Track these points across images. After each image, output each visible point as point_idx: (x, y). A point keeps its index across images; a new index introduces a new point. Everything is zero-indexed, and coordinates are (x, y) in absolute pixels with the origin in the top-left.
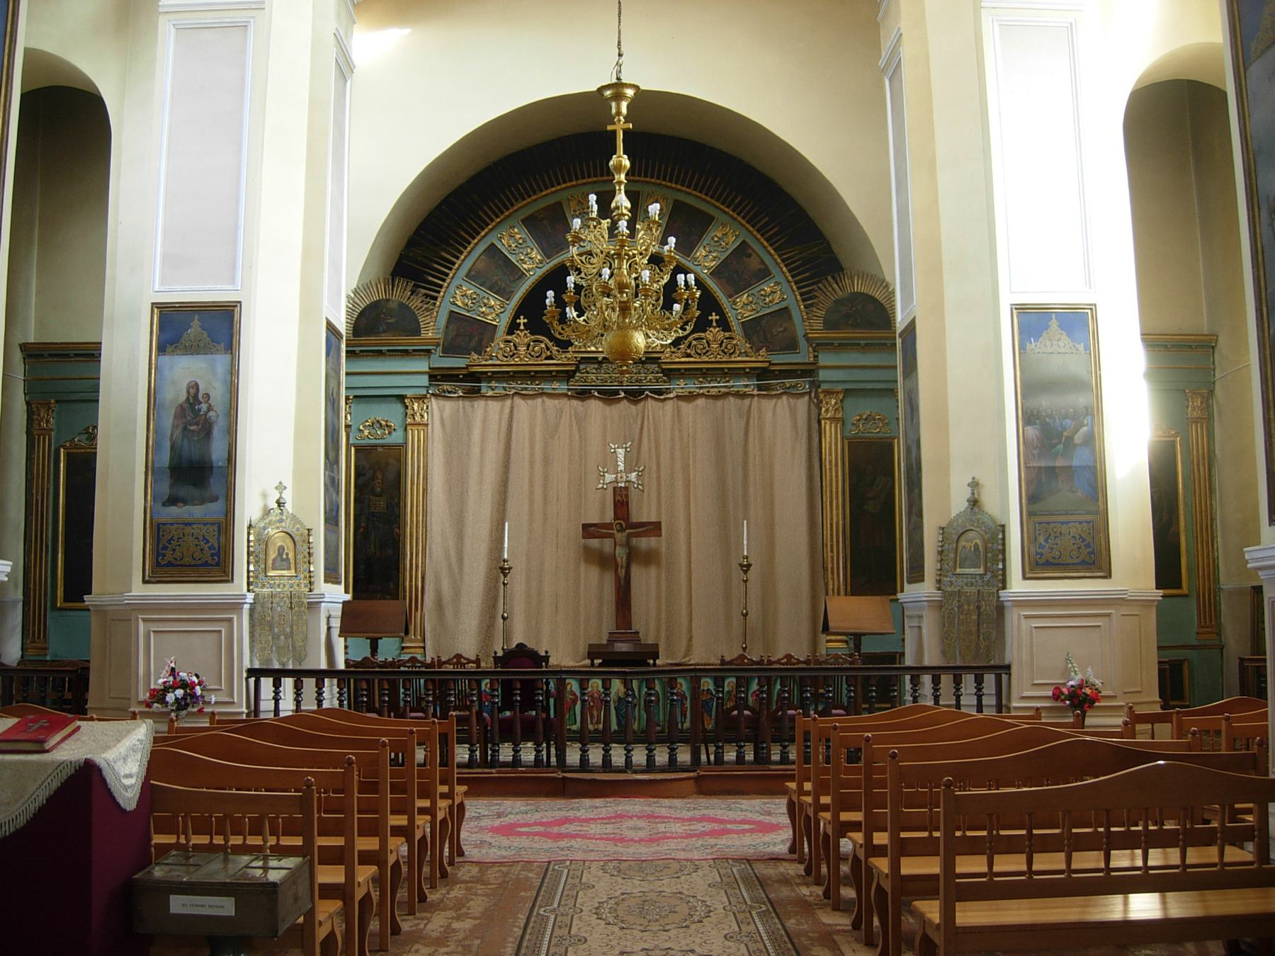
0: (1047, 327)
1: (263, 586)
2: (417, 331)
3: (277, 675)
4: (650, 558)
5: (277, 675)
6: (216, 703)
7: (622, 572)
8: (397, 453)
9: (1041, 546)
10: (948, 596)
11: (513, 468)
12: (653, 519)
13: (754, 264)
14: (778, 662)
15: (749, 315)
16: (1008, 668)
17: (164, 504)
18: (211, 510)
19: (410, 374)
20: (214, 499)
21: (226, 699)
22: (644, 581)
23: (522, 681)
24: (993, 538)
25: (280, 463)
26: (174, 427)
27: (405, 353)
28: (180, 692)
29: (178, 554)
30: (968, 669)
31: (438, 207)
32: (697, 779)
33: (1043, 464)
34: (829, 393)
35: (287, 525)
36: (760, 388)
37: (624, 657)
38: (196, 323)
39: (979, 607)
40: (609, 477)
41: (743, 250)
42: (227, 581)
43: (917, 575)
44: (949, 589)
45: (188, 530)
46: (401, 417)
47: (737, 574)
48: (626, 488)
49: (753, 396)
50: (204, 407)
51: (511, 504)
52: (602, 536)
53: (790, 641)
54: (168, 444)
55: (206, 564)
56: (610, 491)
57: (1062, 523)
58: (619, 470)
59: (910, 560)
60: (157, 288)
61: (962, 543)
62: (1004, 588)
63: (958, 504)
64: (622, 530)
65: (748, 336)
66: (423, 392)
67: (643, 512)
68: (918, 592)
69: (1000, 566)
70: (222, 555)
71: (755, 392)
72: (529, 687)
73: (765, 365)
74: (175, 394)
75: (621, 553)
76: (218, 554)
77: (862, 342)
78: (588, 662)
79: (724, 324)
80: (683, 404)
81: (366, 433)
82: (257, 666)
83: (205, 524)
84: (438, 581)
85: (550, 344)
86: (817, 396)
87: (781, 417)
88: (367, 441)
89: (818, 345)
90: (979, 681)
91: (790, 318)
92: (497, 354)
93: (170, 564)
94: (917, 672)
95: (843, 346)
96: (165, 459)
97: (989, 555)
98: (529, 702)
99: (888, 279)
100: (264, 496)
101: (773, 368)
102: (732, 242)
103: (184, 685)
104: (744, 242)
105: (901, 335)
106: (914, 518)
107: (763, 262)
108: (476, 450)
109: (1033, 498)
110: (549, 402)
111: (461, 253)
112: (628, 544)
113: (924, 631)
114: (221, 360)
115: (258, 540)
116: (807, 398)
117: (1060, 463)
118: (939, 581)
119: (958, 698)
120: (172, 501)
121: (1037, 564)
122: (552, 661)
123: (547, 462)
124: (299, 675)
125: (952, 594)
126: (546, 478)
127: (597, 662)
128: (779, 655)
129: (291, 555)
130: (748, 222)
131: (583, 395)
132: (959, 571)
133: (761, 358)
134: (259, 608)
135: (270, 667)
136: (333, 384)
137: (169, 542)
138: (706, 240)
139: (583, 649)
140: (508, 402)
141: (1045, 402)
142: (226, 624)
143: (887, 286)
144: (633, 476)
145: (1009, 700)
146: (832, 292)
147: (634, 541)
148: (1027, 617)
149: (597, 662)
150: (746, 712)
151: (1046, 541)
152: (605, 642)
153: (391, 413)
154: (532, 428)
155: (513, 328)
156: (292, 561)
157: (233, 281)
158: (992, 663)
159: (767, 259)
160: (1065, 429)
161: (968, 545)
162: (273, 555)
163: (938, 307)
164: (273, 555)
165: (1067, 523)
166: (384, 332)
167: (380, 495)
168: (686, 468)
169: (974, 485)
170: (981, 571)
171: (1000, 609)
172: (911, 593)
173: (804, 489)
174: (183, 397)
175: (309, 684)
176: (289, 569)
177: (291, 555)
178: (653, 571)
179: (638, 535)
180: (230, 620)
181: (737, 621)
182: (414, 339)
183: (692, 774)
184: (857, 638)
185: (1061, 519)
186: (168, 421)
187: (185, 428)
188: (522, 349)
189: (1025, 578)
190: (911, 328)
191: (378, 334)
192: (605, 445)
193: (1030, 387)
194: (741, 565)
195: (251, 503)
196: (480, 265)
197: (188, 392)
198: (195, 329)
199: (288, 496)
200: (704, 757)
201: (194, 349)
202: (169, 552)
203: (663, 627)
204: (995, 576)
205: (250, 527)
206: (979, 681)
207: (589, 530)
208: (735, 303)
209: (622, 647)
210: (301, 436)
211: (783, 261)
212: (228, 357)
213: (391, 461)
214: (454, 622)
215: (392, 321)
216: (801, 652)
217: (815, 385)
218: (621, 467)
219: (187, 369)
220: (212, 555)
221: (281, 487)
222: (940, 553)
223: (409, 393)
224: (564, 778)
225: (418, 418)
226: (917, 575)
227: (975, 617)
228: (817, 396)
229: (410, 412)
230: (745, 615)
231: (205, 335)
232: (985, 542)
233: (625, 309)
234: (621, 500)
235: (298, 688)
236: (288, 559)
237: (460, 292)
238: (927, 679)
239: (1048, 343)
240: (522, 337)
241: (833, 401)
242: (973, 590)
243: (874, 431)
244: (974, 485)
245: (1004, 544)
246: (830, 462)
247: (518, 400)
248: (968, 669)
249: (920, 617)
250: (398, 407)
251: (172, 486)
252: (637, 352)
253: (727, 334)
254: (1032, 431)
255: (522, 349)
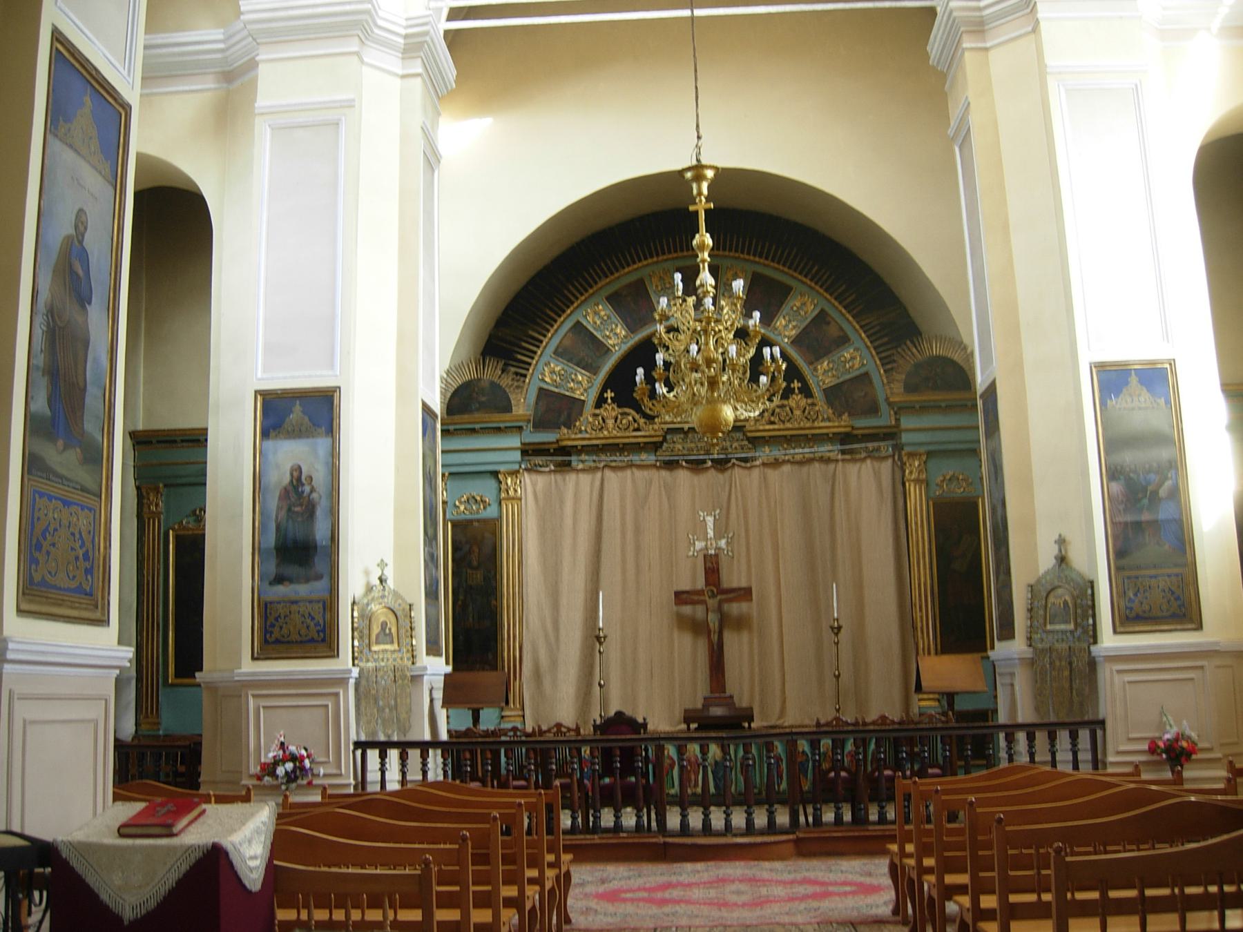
0: (1127, 383)
1: (368, 661)
2: (508, 409)
3: (383, 747)
4: (741, 623)
5: (383, 747)
6: (325, 775)
7: (715, 638)
8: (492, 528)
9: (1130, 600)
10: (1039, 653)
11: (605, 536)
12: (744, 584)
13: (833, 331)
14: (874, 723)
15: (829, 381)
16: (1102, 723)
17: (270, 584)
18: (317, 588)
19: (503, 449)
20: (319, 577)
21: (335, 771)
22: (736, 647)
23: (620, 748)
24: (1083, 594)
25: (382, 542)
26: (279, 509)
27: (498, 430)
28: (289, 766)
29: (285, 631)
30: (1063, 725)
31: (525, 288)
32: (797, 842)
33: (1129, 518)
34: (911, 455)
35: (389, 600)
36: (843, 452)
37: (720, 721)
38: (298, 408)
39: (1070, 664)
40: (699, 545)
41: (821, 318)
42: (332, 657)
43: (1007, 632)
44: (1040, 646)
45: (294, 607)
46: (495, 492)
47: (828, 636)
48: (716, 555)
49: (837, 461)
50: (307, 489)
51: (604, 572)
52: (693, 603)
53: (882, 702)
54: (273, 527)
55: (312, 640)
56: (701, 558)
57: (1151, 577)
58: (708, 536)
59: (1000, 618)
60: (259, 375)
61: (1051, 599)
62: (1095, 642)
63: (1046, 561)
64: (713, 596)
65: (830, 403)
66: (516, 467)
67: (733, 578)
68: (1010, 650)
69: (1091, 621)
70: (328, 631)
71: (840, 457)
72: (629, 755)
73: (848, 430)
74: (279, 477)
75: (713, 619)
76: (324, 631)
77: (943, 404)
78: (684, 726)
79: (806, 391)
80: (770, 472)
81: (462, 508)
82: (363, 738)
83: (311, 602)
84: (535, 651)
85: (637, 417)
86: (900, 458)
87: (865, 481)
88: (463, 517)
89: (900, 408)
90: (1074, 737)
91: (871, 382)
92: (585, 429)
93: (277, 641)
94: (1011, 730)
95: (924, 409)
96: (271, 540)
97: (1079, 611)
98: (628, 769)
99: (966, 340)
100: (367, 573)
101: (855, 432)
102: (811, 311)
103: (293, 758)
104: (822, 311)
105: (981, 396)
106: (1002, 577)
107: (841, 329)
108: (568, 521)
109: (1121, 552)
110: (639, 474)
111: (548, 331)
112: (720, 609)
113: (1017, 688)
114: (323, 443)
115: (362, 616)
116: (890, 461)
117: (1145, 517)
118: (1029, 638)
119: (1053, 754)
120: (279, 580)
121: (1127, 618)
122: (650, 727)
123: (638, 531)
124: (404, 746)
125: (1042, 650)
126: (638, 548)
127: (694, 726)
128: (872, 716)
129: (394, 630)
130: (826, 290)
131: (670, 465)
132: (1049, 627)
133: (842, 424)
134: (363, 682)
135: (376, 739)
136: (430, 462)
137: (276, 619)
138: (785, 309)
139: (678, 714)
140: (599, 475)
141: (1128, 458)
142: (333, 698)
143: (965, 348)
144: (723, 543)
145: (1105, 754)
146: (911, 357)
147: (726, 607)
148: (1119, 672)
149: (694, 726)
150: (843, 774)
151: (1136, 595)
152: (699, 706)
153: (485, 488)
154: (622, 499)
155: (601, 401)
156: (395, 635)
157: (332, 366)
158: (1086, 718)
159: (845, 326)
160: (1149, 483)
161: (1057, 601)
162: (376, 630)
163: (1017, 368)
164: (376, 630)
165: (1155, 577)
166: (478, 410)
167: (477, 568)
168: (774, 533)
169: (1061, 542)
170: (1072, 626)
171: (1092, 664)
172: (1001, 650)
173: (890, 551)
174: (286, 479)
175: (414, 755)
176: (392, 642)
177: (394, 630)
178: (745, 636)
179: (730, 600)
180: (337, 695)
181: (830, 682)
182: (507, 416)
183: (791, 837)
184: (950, 696)
185: (1153, 572)
186: (273, 503)
187: (289, 510)
188: (610, 422)
189: (1115, 632)
190: (991, 390)
191: (471, 412)
192: (695, 513)
193: (1112, 443)
194: (832, 628)
195: (355, 577)
196: (567, 342)
197: (292, 475)
198: (297, 414)
199: (389, 573)
200: (802, 819)
201: (297, 433)
202: (277, 629)
203: (757, 689)
204: (1085, 632)
205: (354, 603)
206: (1074, 737)
207: (681, 597)
208: (816, 369)
209: (717, 711)
210: (400, 513)
211: (861, 327)
212: (330, 440)
213: (487, 535)
214: (552, 693)
215: (484, 399)
216: (895, 714)
217: (898, 448)
218: (711, 533)
219: (290, 453)
220: (318, 632)
221: (382, 565)
222: (1030, 610)
223: (502, 468)
224: (665, 843)
225: (511, 493)
226: (1007, 632)
227: (1066, 673)
228: (900, 458)
229: (503, 487)
230: (838, 677)
231: (307, 419)
232: (1073, 598)
233: (713, 383)
234: (712, 567)
235: (403, 758)
236: (390, 633)
237: (548, 369)
238: (1021, 736)
239: (1129, 400)
240: (610, 410)
241: (917, 463)
242: (1065, 646)
243: (959, 491)
244: (1061, 542)
245: (1093, 600)
246: (916, 523)
247: (608, 473)
248: (1063, 725)
249: (1012, 675)
250: (492, 483)
251: (278, 565)
252: (727, 425)
253: (810, 401)
254: (1116, 487)
255: (610, 422)
